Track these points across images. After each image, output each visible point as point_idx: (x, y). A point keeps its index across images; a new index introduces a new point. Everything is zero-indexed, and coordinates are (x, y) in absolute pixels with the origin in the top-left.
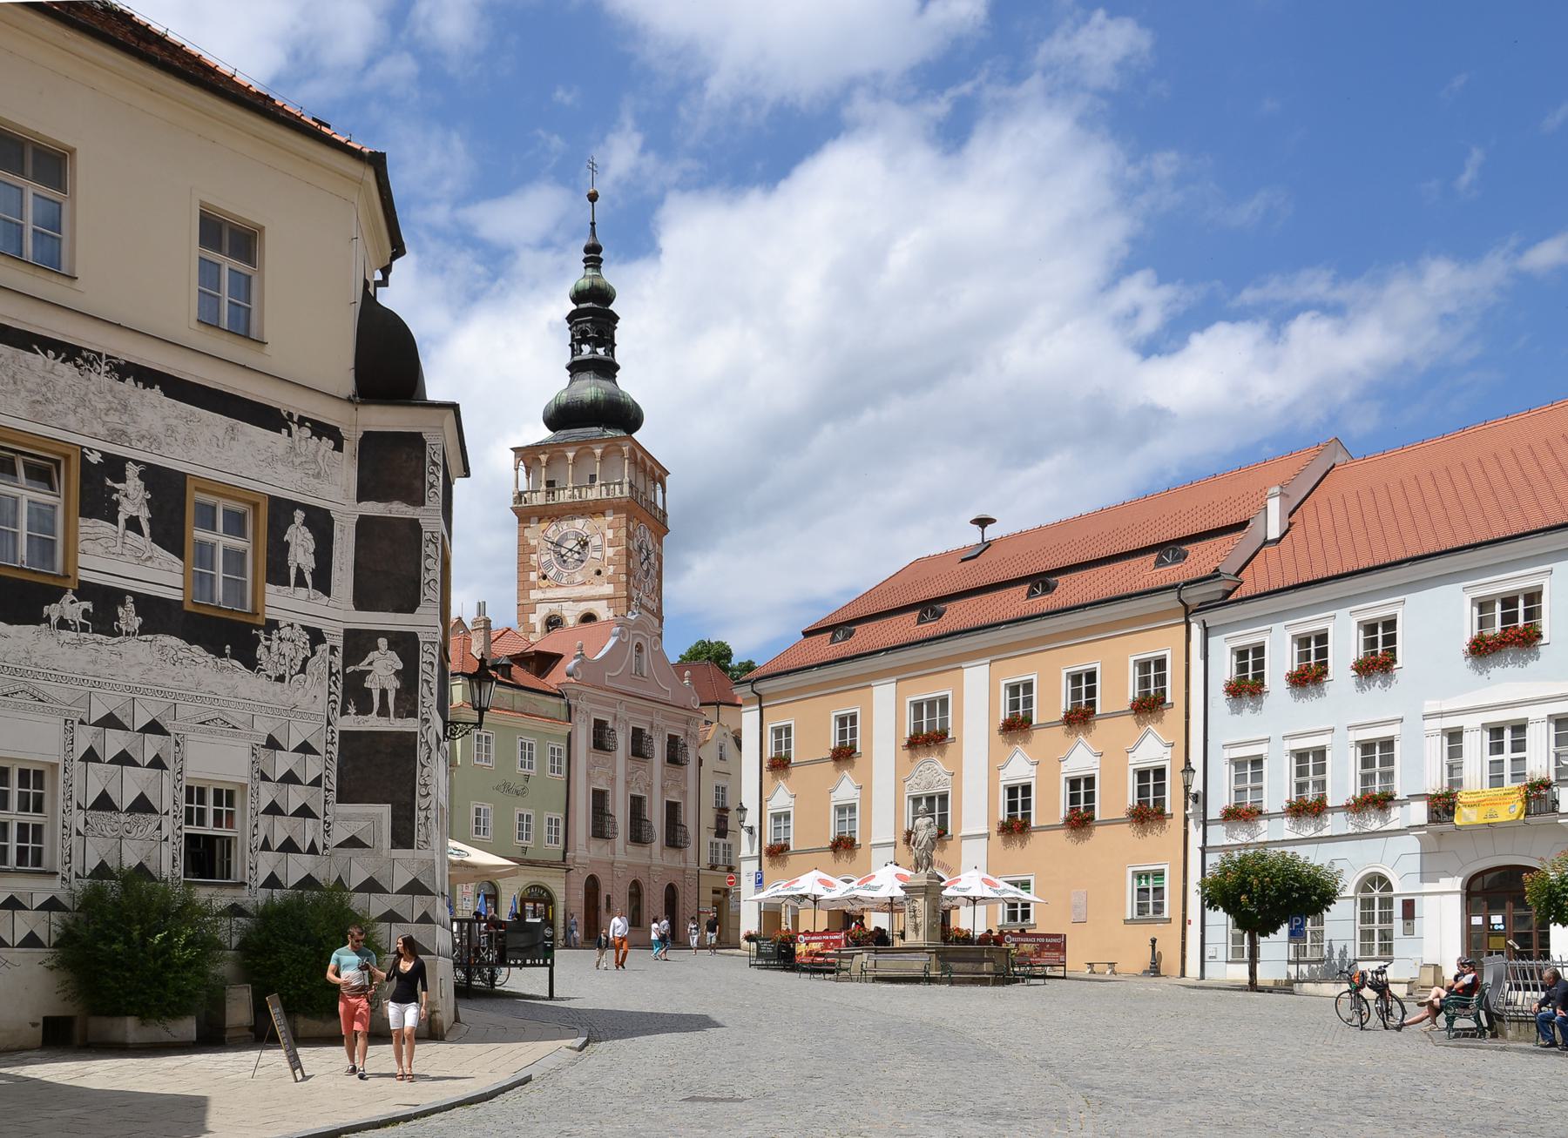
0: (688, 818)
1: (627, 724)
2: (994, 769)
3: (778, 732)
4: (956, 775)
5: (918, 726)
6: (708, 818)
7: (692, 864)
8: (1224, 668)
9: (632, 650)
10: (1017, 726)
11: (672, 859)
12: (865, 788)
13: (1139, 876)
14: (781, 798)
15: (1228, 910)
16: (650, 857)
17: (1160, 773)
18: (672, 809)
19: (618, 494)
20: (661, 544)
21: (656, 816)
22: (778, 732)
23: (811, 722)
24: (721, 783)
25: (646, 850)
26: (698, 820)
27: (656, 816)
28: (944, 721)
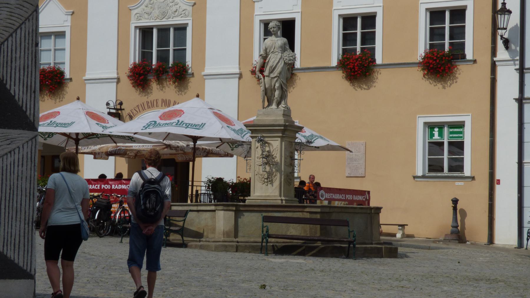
13: (430, 126)
15: (153, 166)
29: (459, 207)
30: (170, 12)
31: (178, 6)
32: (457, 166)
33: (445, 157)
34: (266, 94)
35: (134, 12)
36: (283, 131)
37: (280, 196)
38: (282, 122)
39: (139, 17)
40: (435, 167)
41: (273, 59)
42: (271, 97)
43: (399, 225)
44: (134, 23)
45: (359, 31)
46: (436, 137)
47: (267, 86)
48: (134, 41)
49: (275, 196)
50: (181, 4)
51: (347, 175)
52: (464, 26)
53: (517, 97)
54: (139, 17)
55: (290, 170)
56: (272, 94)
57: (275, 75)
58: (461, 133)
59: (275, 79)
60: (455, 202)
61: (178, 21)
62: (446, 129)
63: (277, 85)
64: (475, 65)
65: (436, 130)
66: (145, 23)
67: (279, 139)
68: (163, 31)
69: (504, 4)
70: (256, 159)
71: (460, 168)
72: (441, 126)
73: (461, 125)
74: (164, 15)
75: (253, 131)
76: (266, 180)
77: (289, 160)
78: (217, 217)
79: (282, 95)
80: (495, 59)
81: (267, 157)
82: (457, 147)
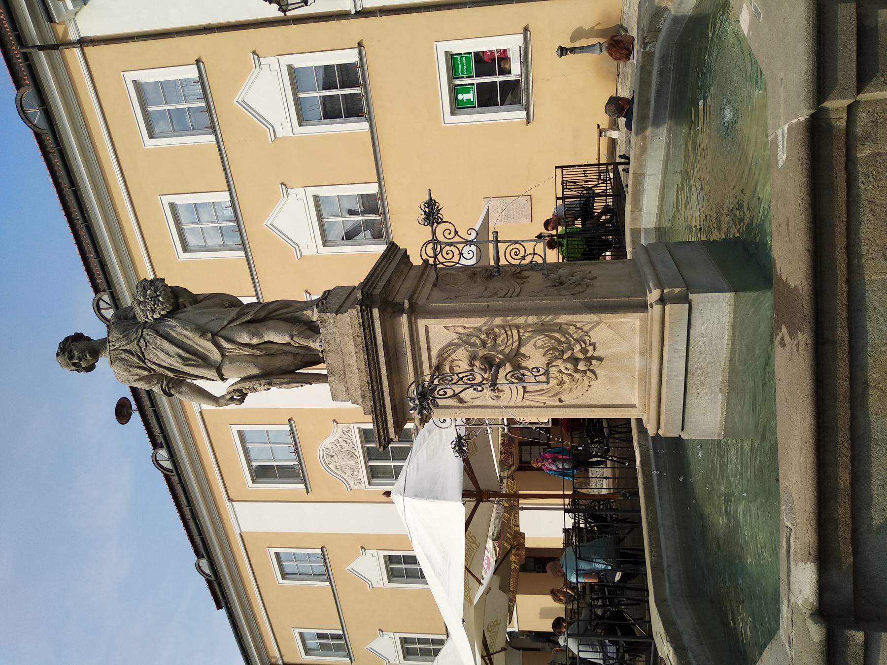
12: (363, 544)
13: (457, 107)
29: (569, 45)
30: (347, 448)
31: (340, 440)
34: (293, 372)
36: (391, 308)
37: (643, 307)
42: (295, 355)
43: (600, 136)
44: (365, 485)
45: (403, 566)
46: (470, 96)
47: (255, 371)
49: (645, 330)
50: (337, 437)
51: (529, 221)
55: (536, 279)
56: (286, 353)
57: (209, 345)
59: (226, 345)
60: (563, 51)
61: (356, 439)
63: (245, 338)
64: (364, 44)
65: (460, 97)
66: (363, 474)
67: (421, 323)
70: (500, 403)
72: (454, 90)
73: (452, 58)
74: (351, 454)
76: (581, 366)
77: (497, 284)
79: (287, 320)
80: (353, 12)
81: (490, 363)
82: (486, 63)
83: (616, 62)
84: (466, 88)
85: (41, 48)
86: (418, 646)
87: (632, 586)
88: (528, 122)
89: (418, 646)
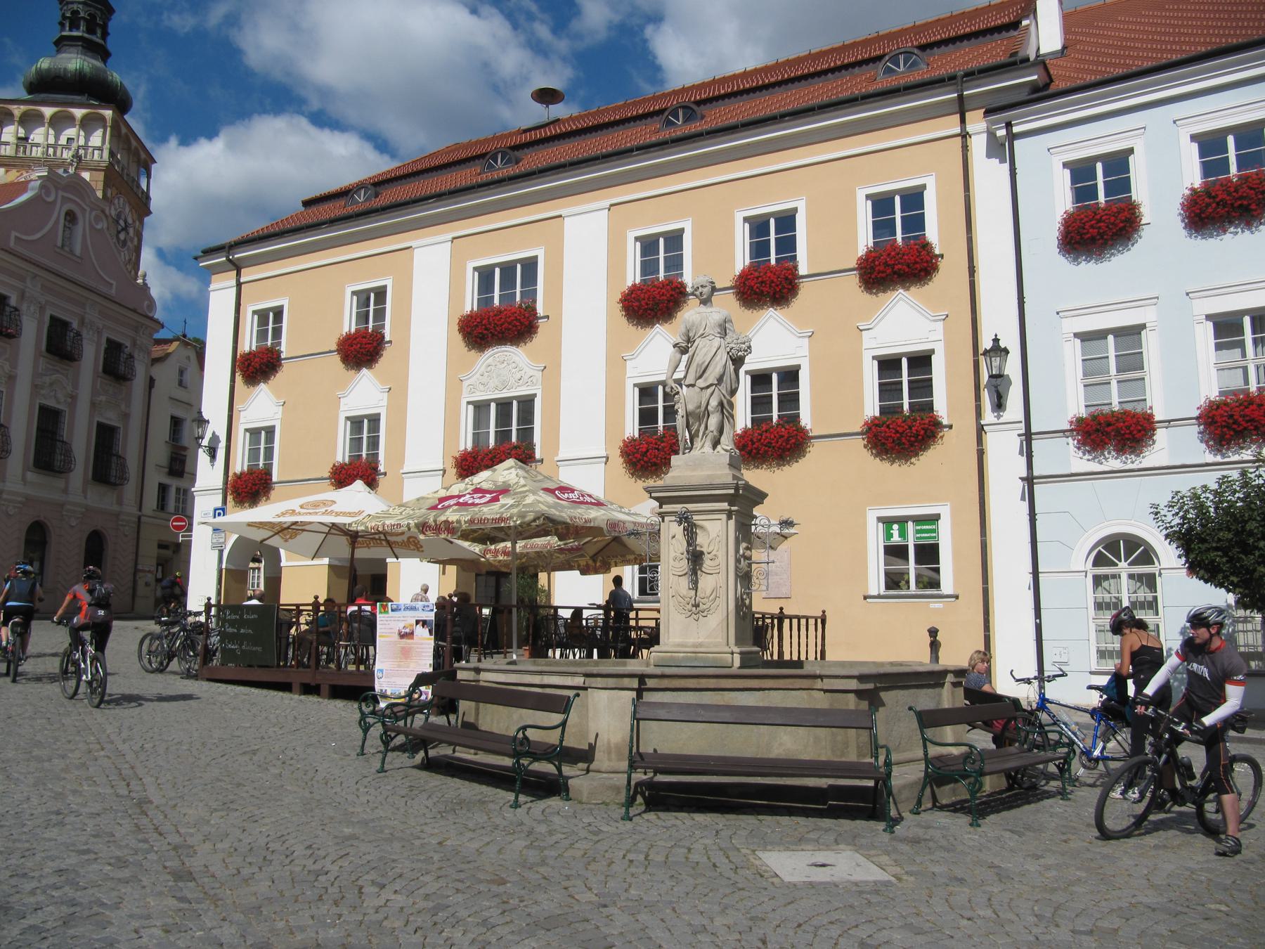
0: (130, 448)
1: (42, 309)
2: (616, 363)
3: (262, 315)
4: (551, 371)
5: (485, 300)
6: (159, 452)
7: (130, 508)
8: (1054, 199)
9: (59, 212)
10: (651, 303)
11: (100, 499)
13: (887, 522)
14: (262, 405)
16: (65, 491)
17: (921, 362)
18: (106, 437)
19: (96, 157)
20: (142, 222)
21: (79, 439)
22: (262, 315)
23: (313, 292)
24: (179, 413)
25: (59, 483)
26: (143, 452)
27: (79, 439)
28: (530, 294)
32: (931, 583)
33: (913, 562)
35: (465, 384)
38: (729, 480)
39: (473, 389)
40: (894, 581)
41: (705, 350)
46: (896, 539)
48: (467, 417)
50: (526, 369)
52: (931, 379)
53: (1024, 475)
54: (473, 389)
58: (933, 531)
60: (933, 632)
62: (910, 524)
63: (714, 403)
68: (504, 406)
69: (996, 340)
71: (935, 584)
72: (902, 521)
73: (935, 518)
75: (662, 501)
78: (590, 707)
80: (983, 422)
82: (929, 554)
83: (334, 347)
84: (903, 534)
85: (961, 97)
86: (262, 446)
87: (489, 667)
88: (865, 598)
89: (262, 446)
